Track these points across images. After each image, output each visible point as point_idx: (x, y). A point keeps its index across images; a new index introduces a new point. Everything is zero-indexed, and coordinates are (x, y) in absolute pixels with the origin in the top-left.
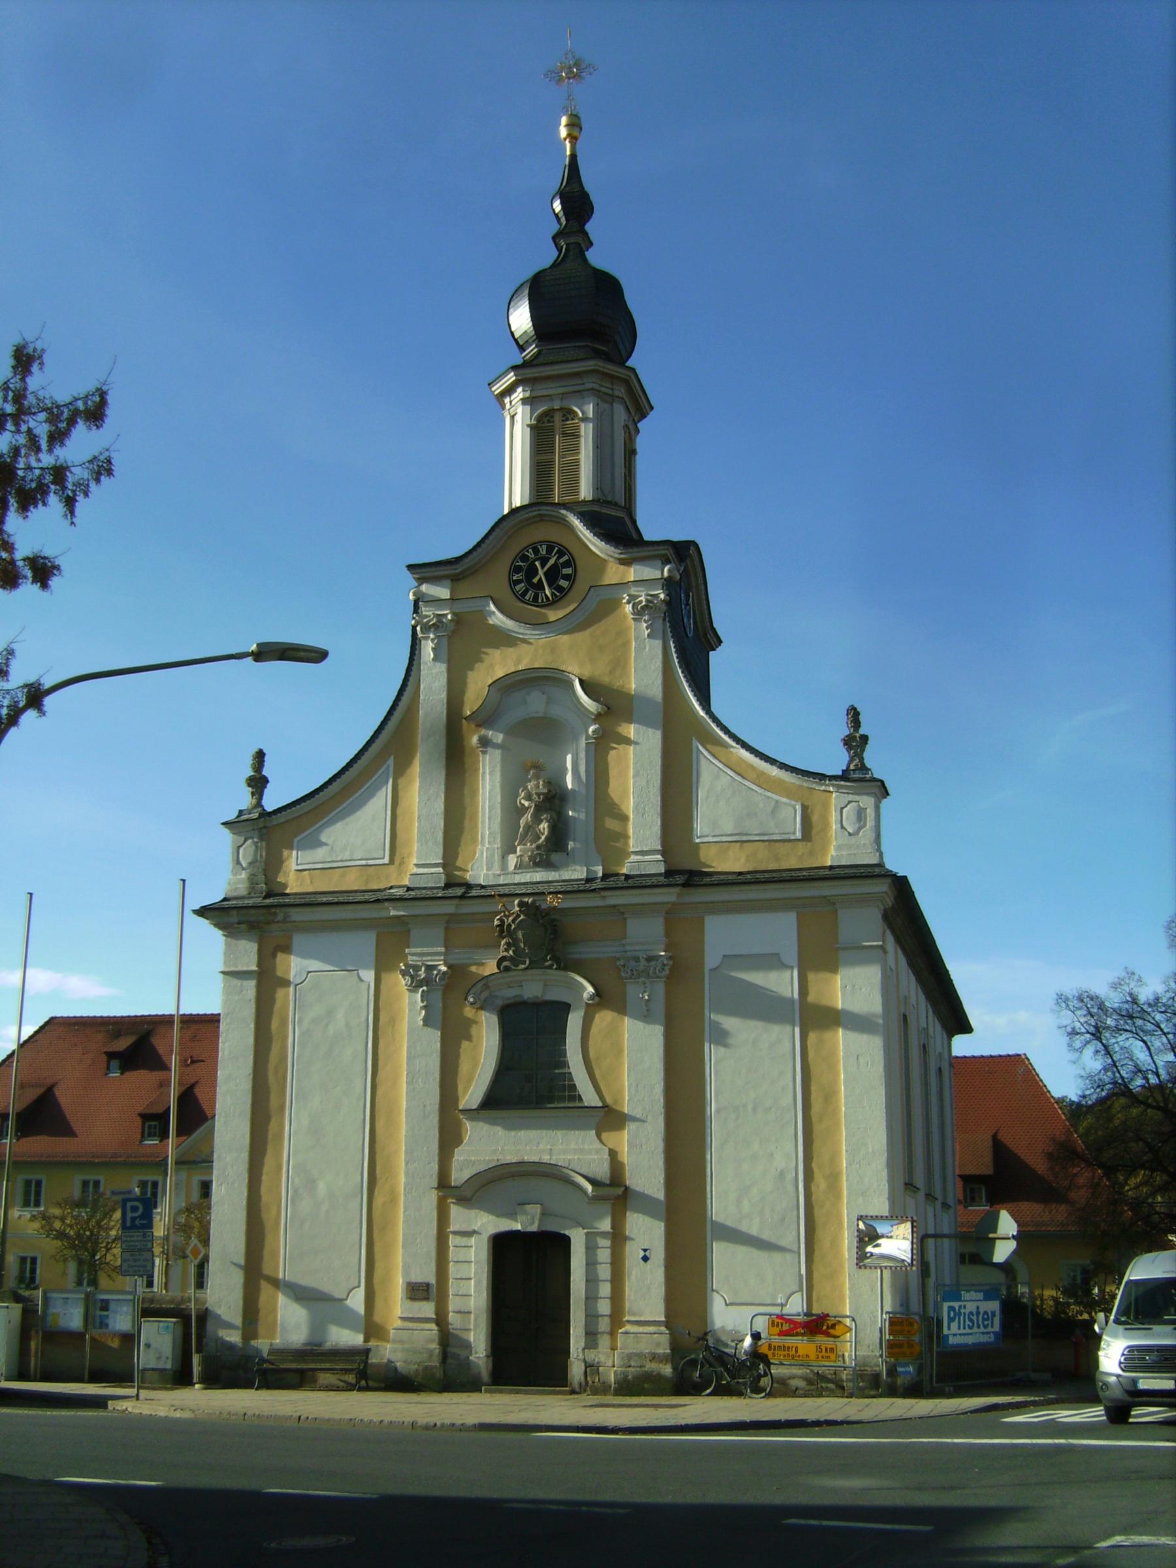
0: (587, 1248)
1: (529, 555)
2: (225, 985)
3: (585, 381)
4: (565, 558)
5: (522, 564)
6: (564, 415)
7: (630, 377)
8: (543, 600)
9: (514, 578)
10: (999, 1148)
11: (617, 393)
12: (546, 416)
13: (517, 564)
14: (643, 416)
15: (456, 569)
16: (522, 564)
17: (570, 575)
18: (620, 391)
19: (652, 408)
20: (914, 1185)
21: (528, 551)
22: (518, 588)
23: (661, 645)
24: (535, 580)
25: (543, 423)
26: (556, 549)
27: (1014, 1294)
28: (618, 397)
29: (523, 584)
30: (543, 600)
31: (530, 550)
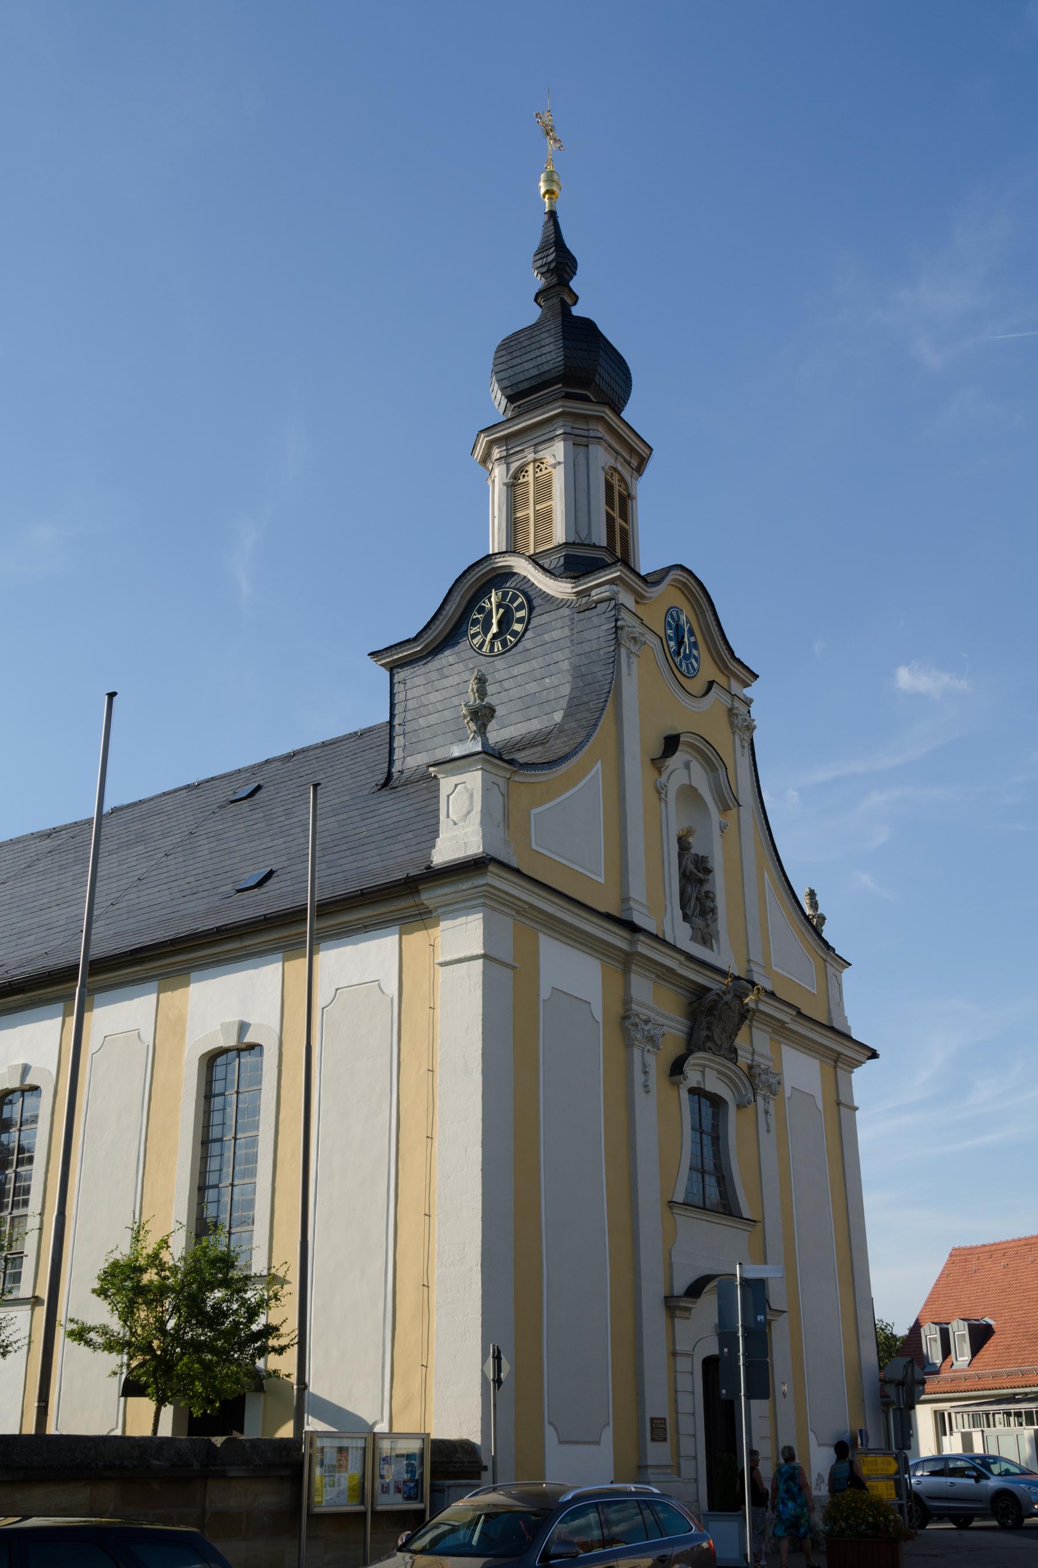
1: (476, 628)
3: (556, 426)
4: (519, 600)
7: (605, 413)
9: (472, 632)
13: (475, 617)
22: (475, 641)
24: (501, 611)
26: (511, 593)
29: (480, 636)
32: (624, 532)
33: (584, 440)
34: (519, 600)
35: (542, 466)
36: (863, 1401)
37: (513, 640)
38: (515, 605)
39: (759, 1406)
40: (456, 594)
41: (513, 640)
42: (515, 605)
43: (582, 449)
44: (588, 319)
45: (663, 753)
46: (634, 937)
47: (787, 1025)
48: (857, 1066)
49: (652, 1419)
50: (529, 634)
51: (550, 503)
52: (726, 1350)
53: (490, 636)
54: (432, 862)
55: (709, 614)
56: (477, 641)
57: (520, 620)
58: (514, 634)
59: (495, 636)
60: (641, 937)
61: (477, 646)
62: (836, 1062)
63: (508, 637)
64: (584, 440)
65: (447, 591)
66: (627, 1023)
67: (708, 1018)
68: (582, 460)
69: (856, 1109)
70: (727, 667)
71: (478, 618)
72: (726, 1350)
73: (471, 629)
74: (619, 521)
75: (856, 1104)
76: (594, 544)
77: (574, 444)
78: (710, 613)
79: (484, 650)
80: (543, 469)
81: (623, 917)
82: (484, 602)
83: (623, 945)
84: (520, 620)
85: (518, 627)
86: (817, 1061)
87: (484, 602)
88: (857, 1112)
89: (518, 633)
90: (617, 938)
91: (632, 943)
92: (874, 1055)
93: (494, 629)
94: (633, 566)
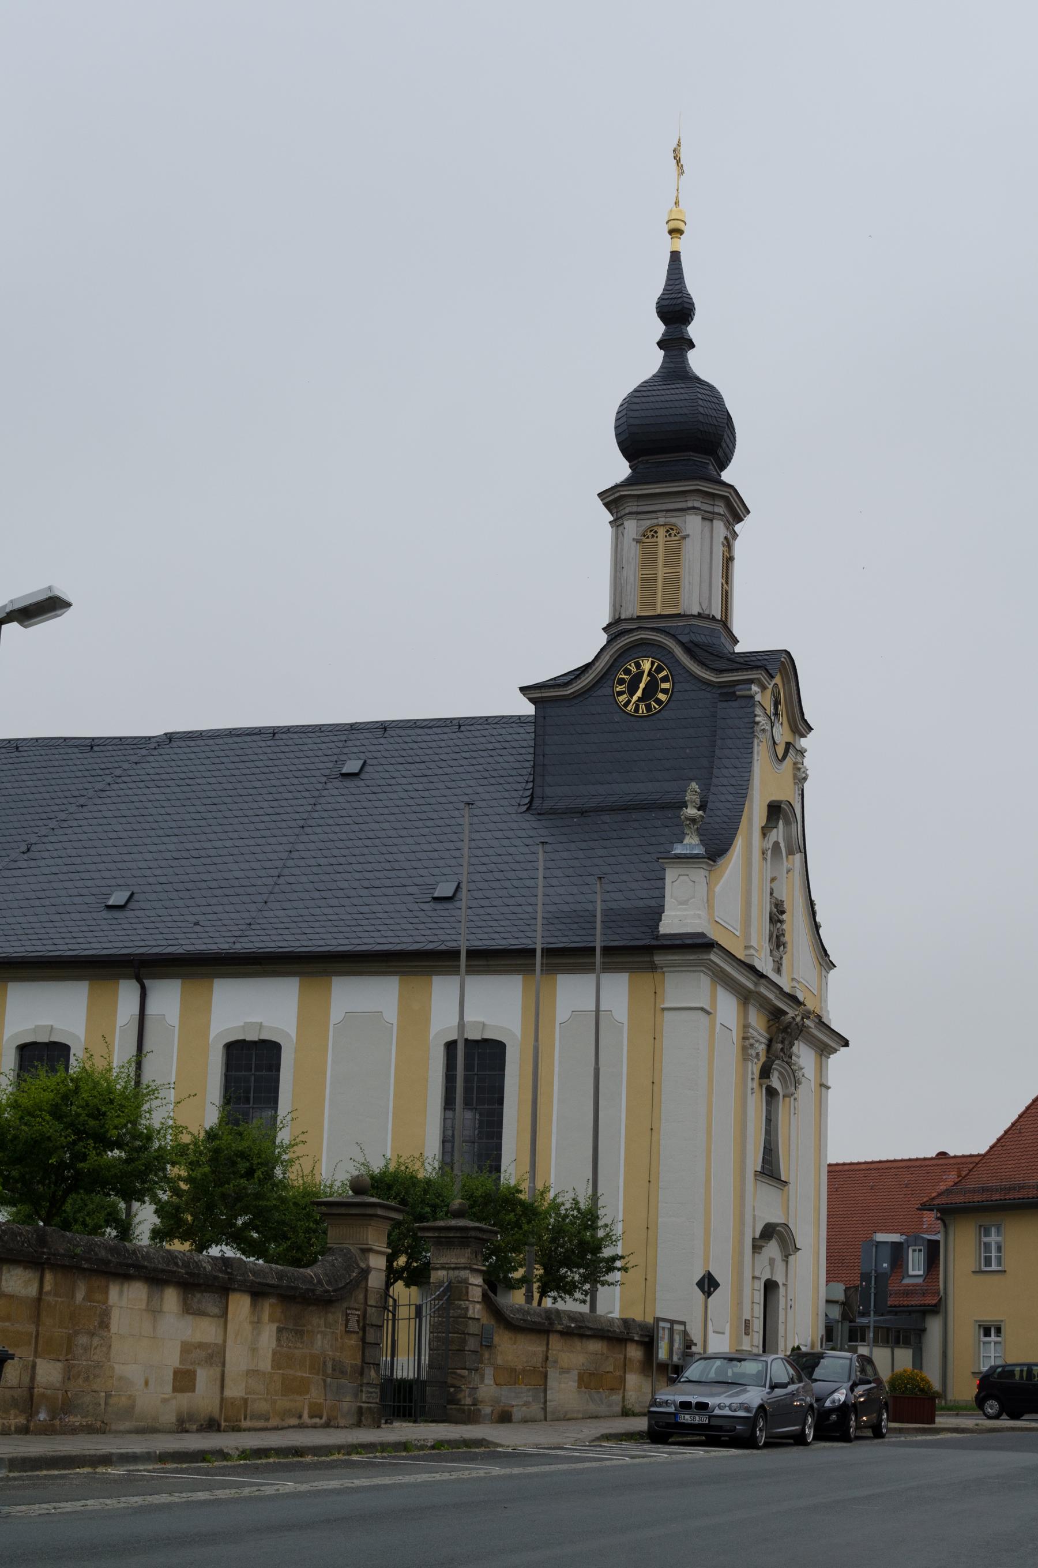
0: (382, 1444)
1: (632, 668)
2: (979, 1393)
3: (688, 498)
4: (664, 673)
5: (625, 677)
6: (667, 531)
7: (730, 493)
8: (643, 711)
9: (618, 689)
10: (799, 1249)
11: (717, 510)
12: (651, 531)
13: (621, 676)
14: (739, 519)
15: (566, 691)
16: (625, 677)
17: (668, 690)
18: (721, 509)
19: (748, 512)
20: (216, 1319)
21: (630, 665)
22: (621, 698)
23: (726, 1351)
25: (648, 537)
27: (307, 1165)
28: (720, 514)
29: (625, 696)
30: (643, 711)
31: (633, 664)
32: (727, 592)
33: (710, 516)
34: (664, 673)
35: (671, 532)
36: (817, 1314)
37: (657, 707)
38: (661, 675)
39: (747, 1315)
40: (605, 654)
41: (657, 707)
42: (661, 675)
43: (707, 523)
44: (711, 388)
45: (767, 821)
46: (759, 980)
47: (810, 1029)
48: (833, 1053)
49: (745, 1320)
50: (672, 705)
51: (678, 570)
52: (864, 1283)
53: (635, 698)
54: (659, 932)
55: (793, 684)
56: (622, 699)
57: (665, 691)
58: (659, 702)
59: (640, 699)
60: (763, 981)
61: (622, 703)
62: (822, 1051)
63: (652, 703)
64: (710, 516)
65: (599, 650)
66: (747, 1043)
67: (783, 1034)
68: (707, 535)
69: (828, 1088)
70: (796, 726)
71: (624, 678)
72: (864, 1283)
73: (617, 687)
74: (725, 585)
75: (829, 1084)
76: (713, 616)
77: (703, 518)
78: (794, 684)
79: (629, 708)
80: (673, 535)
81: (747, 961)
82: (630, 665)
83: (750, 985)
84: (665, 691)
85: (662, 697)
86: (813, 1052)
87: (630, 665)
88: (829, 1090)
89: (663, 702)
90: (746, 981)
91: (756, 984)
92: (846, 1043)
93: (639, 693)
94: (729, 626)
